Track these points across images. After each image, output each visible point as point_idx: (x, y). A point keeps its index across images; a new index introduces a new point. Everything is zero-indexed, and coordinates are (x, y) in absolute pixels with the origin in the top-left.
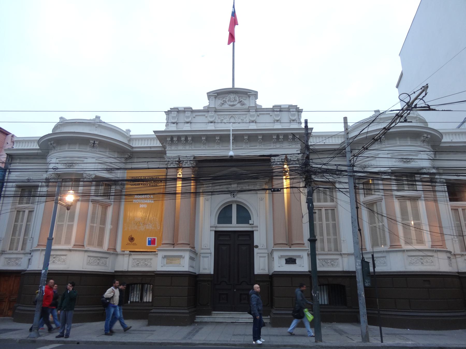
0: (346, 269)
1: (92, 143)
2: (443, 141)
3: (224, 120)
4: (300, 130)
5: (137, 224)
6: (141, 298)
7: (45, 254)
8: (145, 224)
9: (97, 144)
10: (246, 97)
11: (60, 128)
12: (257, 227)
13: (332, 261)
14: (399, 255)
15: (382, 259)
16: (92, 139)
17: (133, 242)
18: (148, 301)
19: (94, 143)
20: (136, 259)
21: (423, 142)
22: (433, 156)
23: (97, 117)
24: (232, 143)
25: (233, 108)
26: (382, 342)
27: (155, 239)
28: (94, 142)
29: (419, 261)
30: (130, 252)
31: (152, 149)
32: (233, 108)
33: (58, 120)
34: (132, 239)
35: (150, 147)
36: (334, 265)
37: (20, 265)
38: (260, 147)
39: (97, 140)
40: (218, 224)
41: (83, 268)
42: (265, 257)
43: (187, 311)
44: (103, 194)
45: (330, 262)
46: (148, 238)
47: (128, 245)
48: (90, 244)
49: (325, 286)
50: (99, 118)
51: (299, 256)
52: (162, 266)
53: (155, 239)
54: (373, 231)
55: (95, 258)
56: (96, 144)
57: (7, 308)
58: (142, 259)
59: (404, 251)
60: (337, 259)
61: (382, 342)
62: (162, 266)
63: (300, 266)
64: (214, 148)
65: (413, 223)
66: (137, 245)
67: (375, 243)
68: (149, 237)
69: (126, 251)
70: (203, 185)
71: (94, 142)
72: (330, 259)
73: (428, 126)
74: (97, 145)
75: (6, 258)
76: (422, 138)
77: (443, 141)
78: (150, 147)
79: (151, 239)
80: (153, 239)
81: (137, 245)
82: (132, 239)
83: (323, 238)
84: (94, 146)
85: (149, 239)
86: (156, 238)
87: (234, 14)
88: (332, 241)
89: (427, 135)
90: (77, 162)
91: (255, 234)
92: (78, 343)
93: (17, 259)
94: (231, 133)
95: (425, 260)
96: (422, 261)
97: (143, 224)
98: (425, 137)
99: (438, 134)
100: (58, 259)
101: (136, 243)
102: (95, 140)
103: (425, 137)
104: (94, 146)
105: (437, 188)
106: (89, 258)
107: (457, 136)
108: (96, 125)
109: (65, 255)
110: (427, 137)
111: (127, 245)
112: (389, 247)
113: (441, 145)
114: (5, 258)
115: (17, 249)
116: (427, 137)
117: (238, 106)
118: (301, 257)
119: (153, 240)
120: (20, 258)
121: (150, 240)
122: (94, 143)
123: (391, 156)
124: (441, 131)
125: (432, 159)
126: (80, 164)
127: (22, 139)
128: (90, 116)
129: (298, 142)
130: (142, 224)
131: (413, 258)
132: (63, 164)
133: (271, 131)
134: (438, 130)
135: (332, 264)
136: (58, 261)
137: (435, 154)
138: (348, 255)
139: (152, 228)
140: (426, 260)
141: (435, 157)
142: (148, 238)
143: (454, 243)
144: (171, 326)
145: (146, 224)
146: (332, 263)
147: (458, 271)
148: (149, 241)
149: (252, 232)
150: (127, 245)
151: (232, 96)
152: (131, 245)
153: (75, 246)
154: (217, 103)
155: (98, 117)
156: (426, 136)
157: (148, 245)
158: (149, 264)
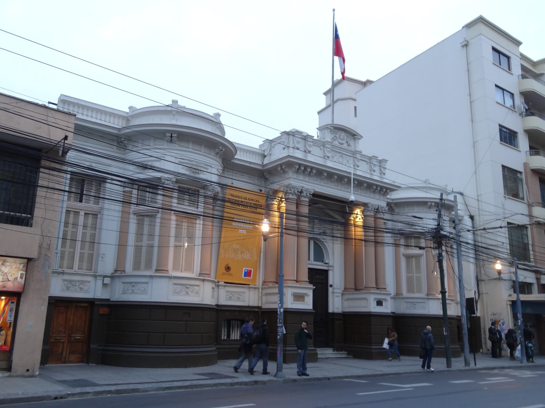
0: (252, 304)
1: (169, 136)
2: (236, 157)
3: (335, 157)
4: (333, 170)
5: (234, 251)
6: (229, 335)
7: (441, 302)
8: (243, 252)
9: (169, 136)
10: (351, 139)
11: (174, 115)
12: (333, 267)
13: (81, 284)
14: (164, 282)
15: (421, 304)
16: (168, 131)
17: (229, 272)
18: (236, 339)
19: (171, 137)
20: (229, 291)
21: (216, 155)
22: (221, 171)
23: (173, 101)
24: (353, 186)
25: (341, 146)
26: (475, 365)
27: (251, 271)
28: (172, 135)
29: (185, 290)
30: (225, 283)
31: (252, 166)
32: (341, 146)
33: (169, 102)
34: (228, 268)
35: (250, 163)
36: (240, 299)
37: (87, 292)
38: (174, 147)
39: (175, 132)
40: (314, 262)
41: (168, 299)
42: (339, 296)
43: (214, 349)
44: (132, 198)
45: (79, 286)
46: (244, 269)
47: (223, 274)
48: (175, 268)
49: (239, 322)
50: (177, 102)
51: (385, 300)
52: (292, 304)
53: (251, 271)
54: (138, 249)
55: (183, 287)
56: (174, 137)
57: (68, 352)
58: (236, 292)
59: (170, 277)
60: (89, 282)
61: (475, 365)
62: (292, 304)
63: (386, 307)
64: (367, 195)
65: (186, 244)
66: (233, 276)
67: (137, 266)
68: (246, 268)
69: (220, 281)
70: (185, 195)
71: (172, 135)
72: (79, 281)
73: (224, 136)
74: (175, 139)
75: (66, 280)
76: (217, 150)
77: (236, 157)
78: (250, 163)
79: (247, 270)
80: (250, 270)
81: (233, 276)
82: (228, 268)
83: (74, 252)
84: (171, 139)
85: (245, 269)
86: (252, 270)
87: (336, 38)
88: (86, 256)
89: (222, 148)
90: (202, 169)
91: (330, 273)
92: (329, 379)
93: (82, 282)
94: (352, 177)
95: (191, 290)
96: (188, 290)
97: (241, 252)
98: (220, 150)
99: (233, 148)
100: (191, 290)
101: (232, 274)
102: (172, 132)
103: (220, 150)
104: (171, 139)
105: (373, 238)
106: (175, 286)
107: (248, 155)
108: (173, 112)
109: (198, 286)
110: (222, 150)
111: (222, 274)
112: (154, 270)
113: (232, 161)
114: (63, 280)
115: (55, 267)
116: (222, 150)
117: (345, 145)
118: (308, 295)
119: (249, 271)
120: (86, 282)
121: (246, 271)
122: (171, 137)
123: (179, 162)
124: (236, 145)
125: (220, 174)
126: (205, 172)
127: (76, 101)
128: (210, 112)
129: (176, 141)
130: (240, 252)
131: (178, 286)
132: (187, 168)
133: (217, 137)
134: (233, 143)
135: (80, 288)
136: (192, 293)
137: (223, 170)
138: (255, 289)
139: (250, 258)
140: (192, 289)
141: (223, 172)
142: (244, 269)
143: (100, 260)
144: (221, 360)
145: (244, 253)
146: (81, 286)
147: (94, 297)
148: (245, 272)
149: (326, 272)
150: (222, 274)
151: (343, 134)
152: (227, 275)
153: (157, 271)
154: (328, 137)
155: (175, 102)
156: (221, 149)
157: (244, 276)
158: (242, 298)
